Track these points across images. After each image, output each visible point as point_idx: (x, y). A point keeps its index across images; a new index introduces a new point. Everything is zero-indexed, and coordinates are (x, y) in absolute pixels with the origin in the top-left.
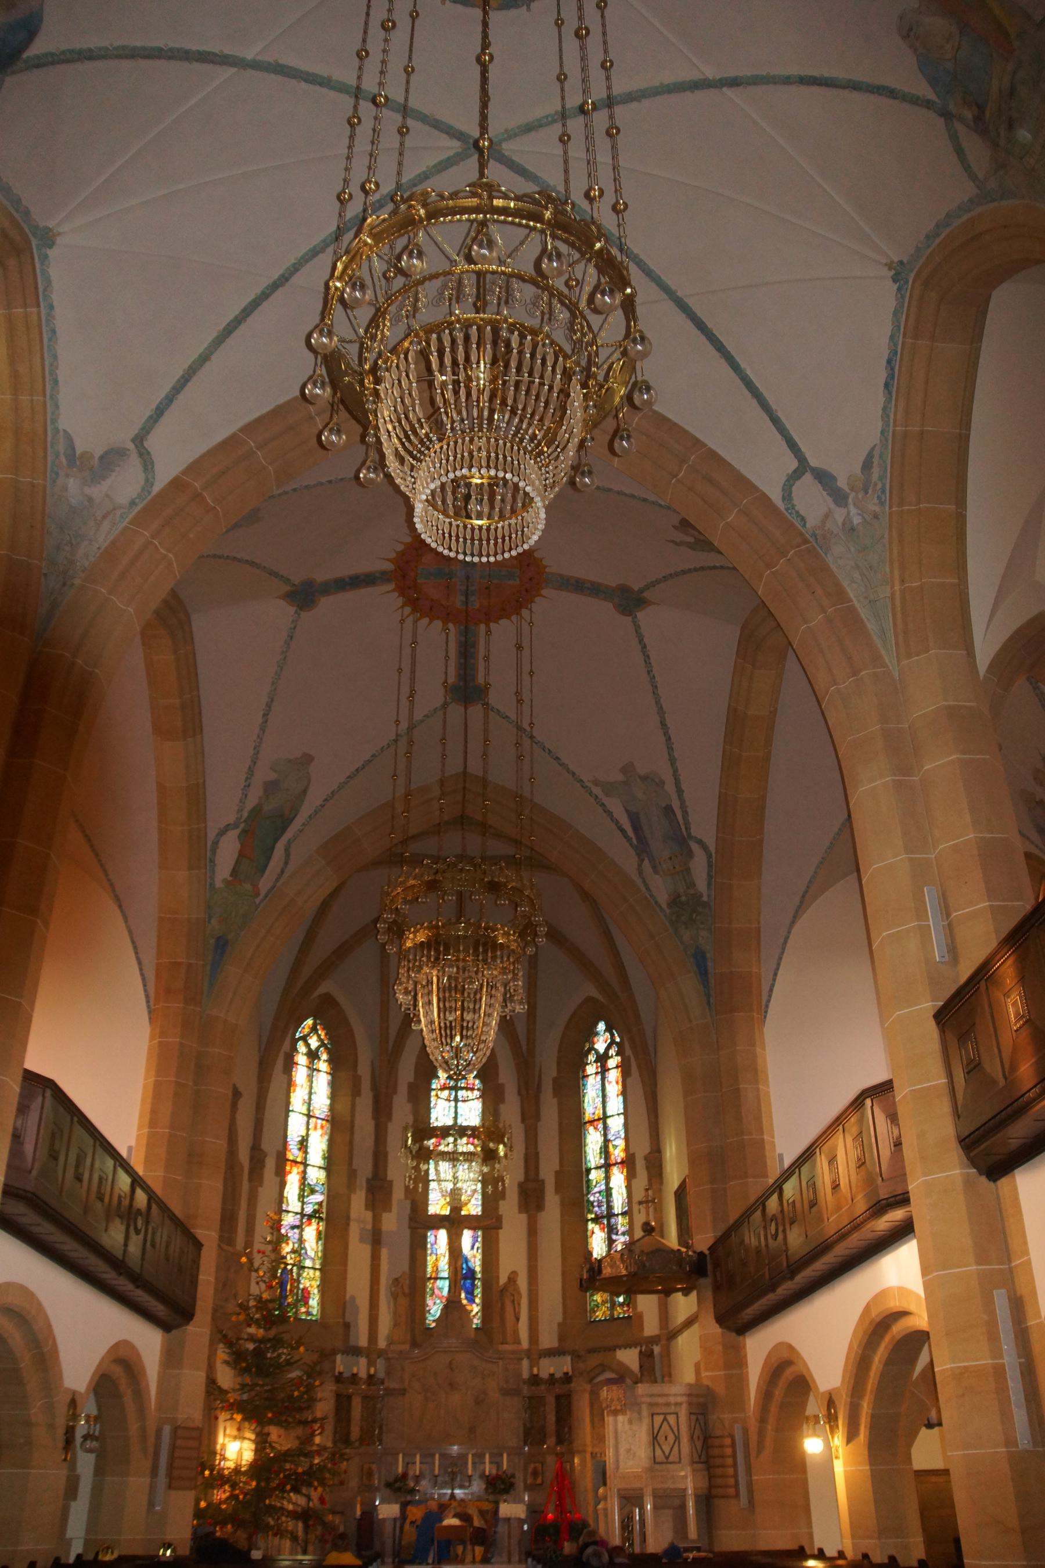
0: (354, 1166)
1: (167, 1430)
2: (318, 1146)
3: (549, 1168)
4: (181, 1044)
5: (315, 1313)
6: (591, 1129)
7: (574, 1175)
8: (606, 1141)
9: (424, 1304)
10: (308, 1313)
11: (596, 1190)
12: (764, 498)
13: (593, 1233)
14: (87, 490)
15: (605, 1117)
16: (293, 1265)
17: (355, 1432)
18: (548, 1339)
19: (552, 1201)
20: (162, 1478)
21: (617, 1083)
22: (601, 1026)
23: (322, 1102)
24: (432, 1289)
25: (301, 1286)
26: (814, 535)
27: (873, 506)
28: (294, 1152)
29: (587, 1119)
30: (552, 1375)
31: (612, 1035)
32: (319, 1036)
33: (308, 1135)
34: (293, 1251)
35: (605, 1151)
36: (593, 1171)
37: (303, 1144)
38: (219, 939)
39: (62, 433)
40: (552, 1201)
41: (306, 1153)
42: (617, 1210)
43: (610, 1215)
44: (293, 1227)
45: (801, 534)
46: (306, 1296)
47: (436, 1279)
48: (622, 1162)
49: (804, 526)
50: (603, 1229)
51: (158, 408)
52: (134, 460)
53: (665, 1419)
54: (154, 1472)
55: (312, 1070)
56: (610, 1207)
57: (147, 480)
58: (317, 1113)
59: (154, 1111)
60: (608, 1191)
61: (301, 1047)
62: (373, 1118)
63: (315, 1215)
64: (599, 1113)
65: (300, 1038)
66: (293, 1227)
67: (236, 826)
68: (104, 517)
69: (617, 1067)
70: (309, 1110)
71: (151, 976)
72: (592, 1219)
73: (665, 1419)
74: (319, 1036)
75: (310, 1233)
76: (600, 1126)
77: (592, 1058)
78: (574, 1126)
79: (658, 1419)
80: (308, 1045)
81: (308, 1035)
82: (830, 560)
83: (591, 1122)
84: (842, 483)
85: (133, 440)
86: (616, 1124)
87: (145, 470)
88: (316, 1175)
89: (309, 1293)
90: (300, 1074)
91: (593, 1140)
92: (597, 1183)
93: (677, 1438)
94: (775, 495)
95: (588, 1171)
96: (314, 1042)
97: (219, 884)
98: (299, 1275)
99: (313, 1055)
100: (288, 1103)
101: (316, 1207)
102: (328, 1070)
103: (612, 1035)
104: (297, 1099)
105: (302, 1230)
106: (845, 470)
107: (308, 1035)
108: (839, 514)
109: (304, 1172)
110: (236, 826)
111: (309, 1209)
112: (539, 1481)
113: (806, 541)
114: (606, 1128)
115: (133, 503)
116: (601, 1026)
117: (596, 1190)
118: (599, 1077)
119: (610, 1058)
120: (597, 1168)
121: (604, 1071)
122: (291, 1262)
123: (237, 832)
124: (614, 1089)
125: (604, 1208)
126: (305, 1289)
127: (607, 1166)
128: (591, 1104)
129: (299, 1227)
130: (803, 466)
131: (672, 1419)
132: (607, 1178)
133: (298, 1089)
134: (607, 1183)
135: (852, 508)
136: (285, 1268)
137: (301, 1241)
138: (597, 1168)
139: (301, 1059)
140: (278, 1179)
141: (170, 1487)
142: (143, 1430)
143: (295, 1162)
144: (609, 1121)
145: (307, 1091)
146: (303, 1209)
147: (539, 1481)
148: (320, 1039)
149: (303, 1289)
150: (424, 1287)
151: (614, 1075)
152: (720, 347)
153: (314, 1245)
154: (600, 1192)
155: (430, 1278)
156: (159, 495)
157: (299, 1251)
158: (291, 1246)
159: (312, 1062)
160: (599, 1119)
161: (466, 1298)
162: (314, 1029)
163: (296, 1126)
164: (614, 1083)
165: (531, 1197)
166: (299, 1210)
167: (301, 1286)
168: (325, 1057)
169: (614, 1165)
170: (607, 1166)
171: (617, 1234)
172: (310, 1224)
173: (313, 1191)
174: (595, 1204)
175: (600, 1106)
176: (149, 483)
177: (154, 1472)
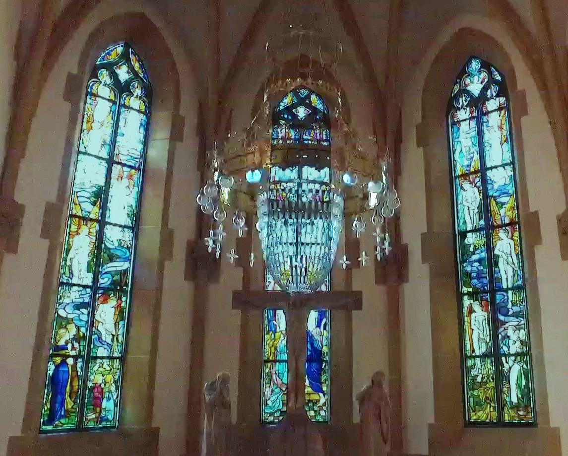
0: (46, 243)
5: (110, 417)
8: (486, 197)
9: (259, 394)
10: (100, 419)
11: (475, 257)
13: (471, 311)
15: (483, 170)
16: (75, 358)
19: (419, 272)
21: (501, 128)
22: (475, 65)
24: (270, 376)
25: (90, 384)
29: (459, 172)
31: (490, 73)
34: (77, 338)
35: (485, 210)
36: (469, 235)
37: (101, 196)
40: (419, 272)
43: (494, 287)
44: (78, 307)
46: (97, 396)
47: (275, 361)
48: (512, 224)
50: (484, 308)
55: (118, 108)
58: (123, 159)
60: (492, 261)
62: (198, 170)
63: (117, 287)
64: (476, 164)
65: (103, 66)
66: (78, 307)
69: (500, 109)
72: (469, 294)
75: (106, 313)
77: (463, 101)
80: (114, 75)
81: (116, 63)
83: (465, 176)
89: (102, 392)
91: (469, 196)
92: (475, 249)
95: (464, 234)
96: (123, 74)
98: (86, 369)
99: (121, 89)
101: (117, 277)
102: (143, 109)
103: (490, 73)
105: (94, 309)
107: (116, 63)
111: (105, 281)
114: (484, 180)
116: (475, 65)
117: (475, 257)
118: (473, 123)
119: (488, 100)
120: (474, 231)
121: (480, 117)
122: (73, 353)
126: (96, 386)
127: (489, 229)
128: (464, 151)
129: (91, 307)
136: (64, 363)
137: (92, 323)
138: (474, 231)
140: (46, 243)
143: (86, 219)
144: (489, 174)
145: (109, 130)
146: (95, 280)
148: (131, 69)
149: (92, 389)
150: (261, 372)
151: (495, 120)
153: (111, 328)
154: (480, 261)
155: (266, 362)
157: (88, 337)
158: (73, 330)
160: (475, 172)
161: (311, 386)
162: (125, 57)
163: (88, 174)
164: (496, 129)
166: (88, 281)
167: (90, 384)
168: (138, 92)
169: (500, 227)
170: (489, 229)
171: (506, 315)
172: (105, 301)
173: (112, 258)
174: (474, 275)
175: (476, 157)
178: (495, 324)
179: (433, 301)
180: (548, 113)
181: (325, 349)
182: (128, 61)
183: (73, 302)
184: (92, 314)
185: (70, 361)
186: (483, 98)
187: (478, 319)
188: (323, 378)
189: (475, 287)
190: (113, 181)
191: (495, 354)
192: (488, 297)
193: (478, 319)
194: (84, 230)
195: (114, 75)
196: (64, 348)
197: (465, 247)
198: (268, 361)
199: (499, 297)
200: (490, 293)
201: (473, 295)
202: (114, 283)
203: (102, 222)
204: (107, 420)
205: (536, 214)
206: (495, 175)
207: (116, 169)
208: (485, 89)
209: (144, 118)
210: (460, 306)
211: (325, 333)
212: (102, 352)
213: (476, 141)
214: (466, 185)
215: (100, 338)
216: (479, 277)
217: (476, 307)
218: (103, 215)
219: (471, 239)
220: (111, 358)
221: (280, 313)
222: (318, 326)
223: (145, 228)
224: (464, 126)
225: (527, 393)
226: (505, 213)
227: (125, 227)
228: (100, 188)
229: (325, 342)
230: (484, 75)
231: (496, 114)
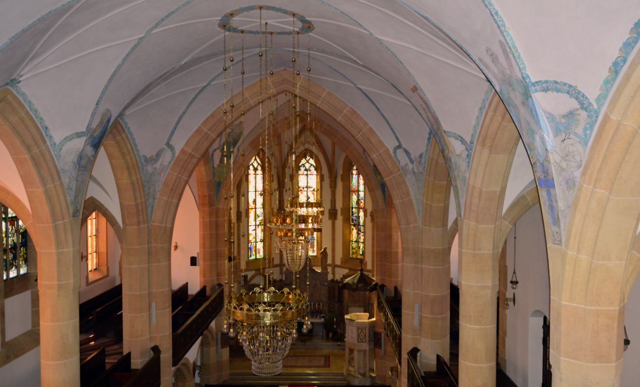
1: (219, 334)
2: (260, 200)
3: (339, 205)
4: (210, 221)
6: (354, 194)
7: (347, 209)
12: (387, 150)
13: (353, 229)
14: (154, 166)
18: (338, 262)
19: (340, 218)
20: (219, 346)
23: (260, 187)
26: (402, 169)
27: (421, 169)
28: (251, 205)
32: (257, 162)
33: (256, 198)
35: (358, 202)
37: (255, 201)
38: (218, 183)
39: (142, 157)
40: (340, 218)
41: (255, 204)
42: (361, 224)
43: (359, 225)
45: (398, 167)
49: (399, 163)
50: (356, 229)
51: (172, 132)
52: (168, 150)
53: (362, 331)
54: (217, 344)
56: (359, 223)
57: (173, 153)
59: (204, 244)
60: (359, 217)
61: (251, 167)
62: (331, 187)
66: (253, 230)
67: (219, 148)
68: (162, 171)
70: (256, 189)
71: (197, 199)
73: (362, 331)
74: (257, 162)
76: (357, 194)
78: (348, 191)
79: (360, 331)
80: (253, 166)
82: (406, 179)
84: (412, 157)
85: (165, 145)
86: (362, 194)
87: (172, 150)
88: (260, 211)
90: (251, 178)
91: (354, 198)
93: (365, 336)
94: (391, 151)
96: (255, 165)
97: (216, 166)
99: (255, 169)
100: (248, 188)
104: (251, 188)
106: (415, 155)
108: (410, 166)
109: (255, 211)
110: (219, 148)
111: (258, 223)
113: (399, 170)
115: (170, 163)
118: (357, 176)
123: (219, 150)
124: (362, 182)
125: (357, 222)
130: (399, 147)
131: (364, 331)
132: (358, 213)
133: (251, 183)
134: (358, 214)
135: (414, 165)
139: (251, 171)
140: (272, 207)
141: (222, 348)
142: (213, 338)
152: (373, 103)
154: (356, 216)
156: (178, 157)
159: (255, 172)
165: (333, 215)
172: (258, 228)
173: (259, 217)
176: (174, 154)
177: (217, 344)
178: (358, 234)
179: (343, 226)
187: (355, 232)
191: (357, 242)
193: (355, 232)
195: (253, 166)
197: (352, 212)
199: (359, 227)
200: (357, 225)
201: (354, 225)
203: (255, 208)
206: (178, 249)
210: (350, 228)
214: (354, 194)
216: (355, 221)
217: (354, 228)
218: (256, 206)
219: (354, 210)
221: (259, 251)
225: (364, 252)
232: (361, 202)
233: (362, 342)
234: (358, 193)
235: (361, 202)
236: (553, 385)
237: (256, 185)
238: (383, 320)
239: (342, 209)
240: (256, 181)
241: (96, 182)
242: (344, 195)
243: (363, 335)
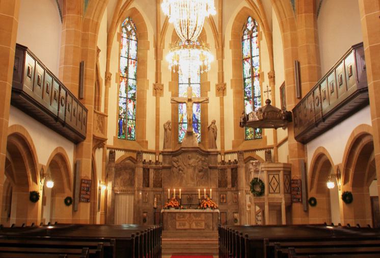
5: (133, 137)
6: (246, 62)
8: (252, 67)
9: (178, 133)
10: (131, 137)
17: (151, 182)
19: (230, 92)
30: (230, 161)
33: (128, 66)
37: (126, 70)
40: (230, 92)
58: (132, 57)
60: (253, 87)
66: (123, 104)
70: (128, 56)
75: (131, 106)
77: (246, 32)
80: (127, 29)
89: (131, 129)
91: (247, 66)
93: (279, 184)
101: (133, 95)
111: (130, 96)
112: (225, 201)
114: (252, 61)
117: (248, 87)
118: (249, 40)
125: (251, 94)
127: (253, 77)
138: (248, 78)
143: (123, 77)
144: (253, 58)
146: (127, 96)
147: (225, 201)
149: (128, 128)
150: (178, 127)
153: (132, 111)
154: (249, 88)
166: (125, 96)
168: (134, 34)
170: (253, 77)
171: (256, 105)
172: (130, 102)
173: (131, 89)
175: (249, 52)
180: (178, 91)
181: (199, 119)
182: (130, 24)
183: (125, 103)
184: (127, 106)
185: (123, 119)
186: (252, 31)
188: (199, 128)
189: (248, 97)
190: (129, 65)
192: (251, 100)
194: (123, 80)
195: (127, 29)
196: (121, 115)
198: (180, 123)
202: (132, 97)
204: (133, 138)
205: (263, 72)
207: (130, 60)
208: (253, 28)
209: (136, 42)
211: (248, 209)
212: (130, 118)
213: (249, 47)
214: (246, 62)
215: (129, 114)
218: (128, 76)
219: (247, 81)
220: (132, 120)
222: (197, 111)
223: (377, 117)
224: (246, 41)
226: (256, 72)
227: (134, 79)
228: (126, 67)
229: (199, 117)
230: (252, 23)
231: (256, 38)
232: (256, 69)
233: (274, 192)
234: (252, 59)
235: (256, 69)
236: (215, 1)
237: (128, 51)
238: (326, 107)
239: (148, 49)
240: (129, 47)
241: (134, 79)
242: (234, 63)
243: (276, 184)
